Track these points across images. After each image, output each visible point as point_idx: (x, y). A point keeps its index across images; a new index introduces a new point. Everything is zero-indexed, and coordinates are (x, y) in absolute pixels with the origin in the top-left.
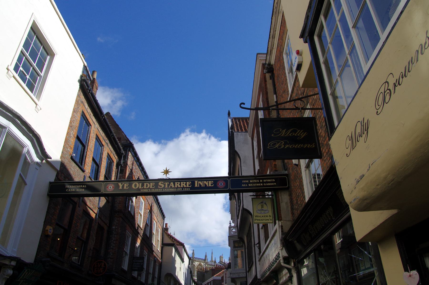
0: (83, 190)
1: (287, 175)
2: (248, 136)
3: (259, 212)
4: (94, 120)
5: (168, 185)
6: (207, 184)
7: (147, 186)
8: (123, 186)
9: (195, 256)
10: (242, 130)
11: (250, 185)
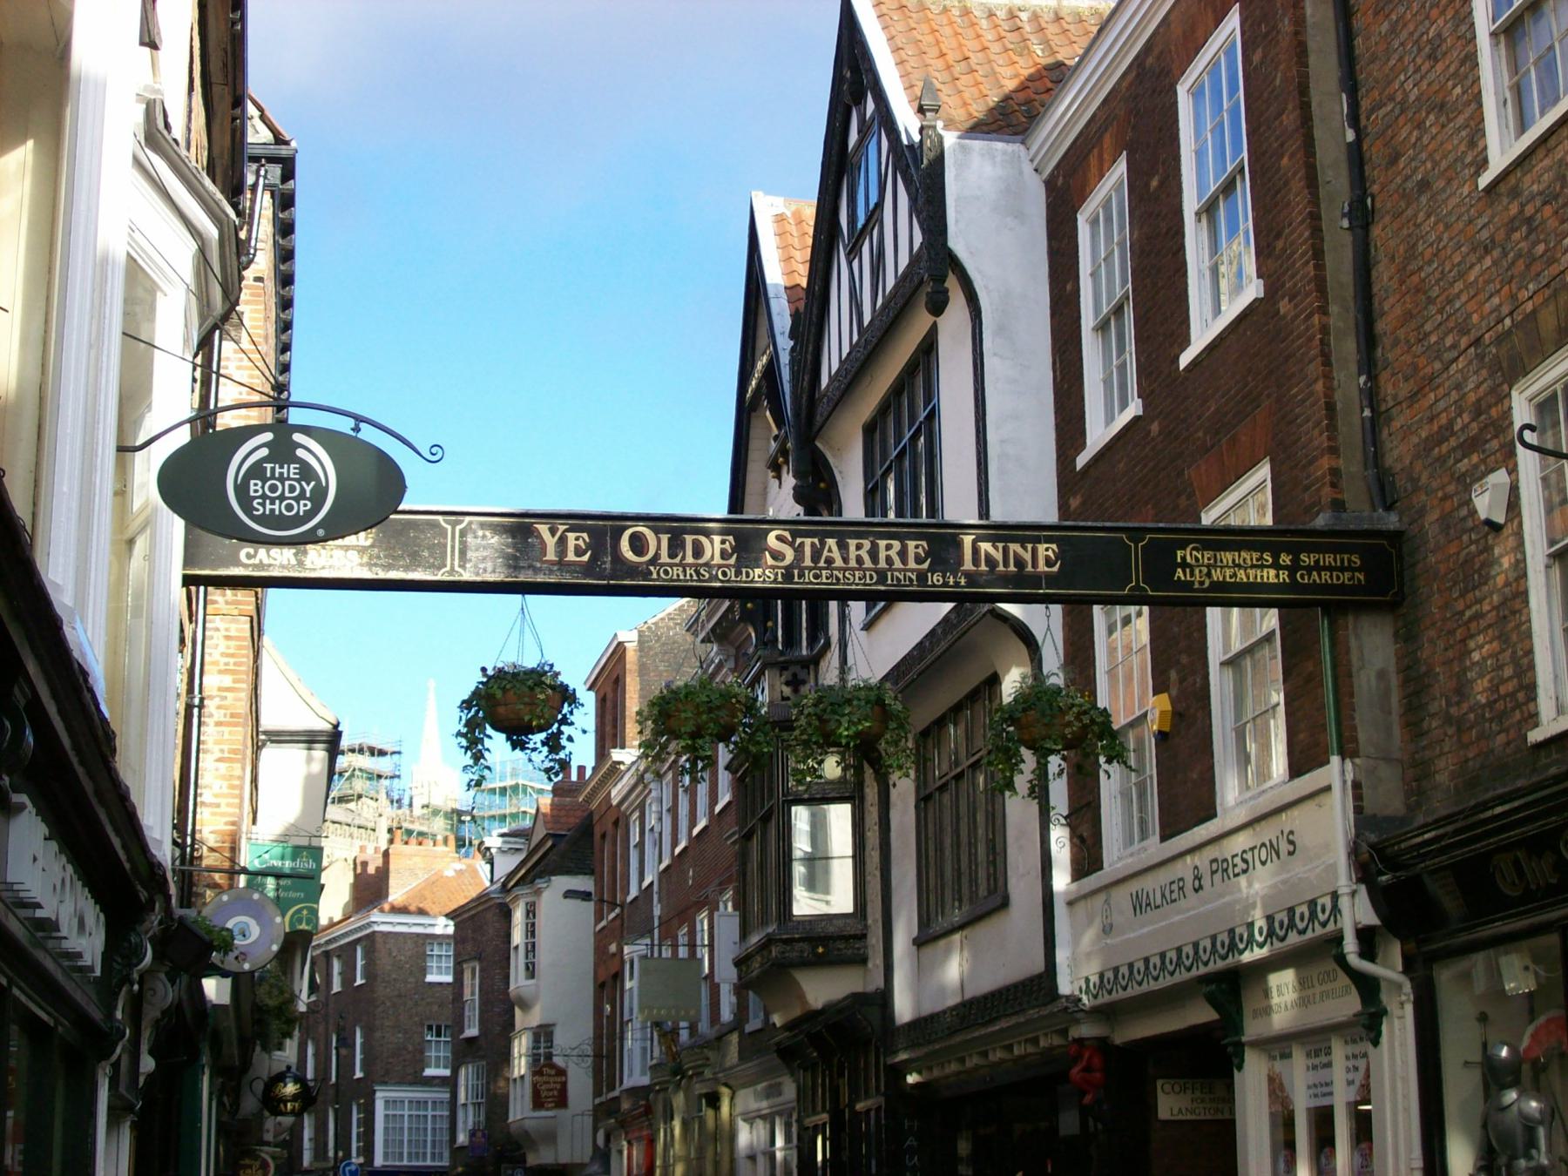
1: (1396, 537)
5: (816, 555)
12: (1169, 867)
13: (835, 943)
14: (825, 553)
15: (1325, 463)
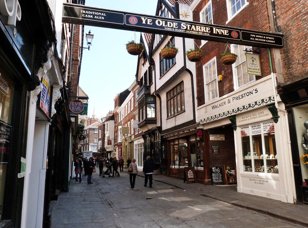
3: (251, 65)
8: (146, 21)
12: (222, 100)
13: (153, 121)
15: (268, 25)
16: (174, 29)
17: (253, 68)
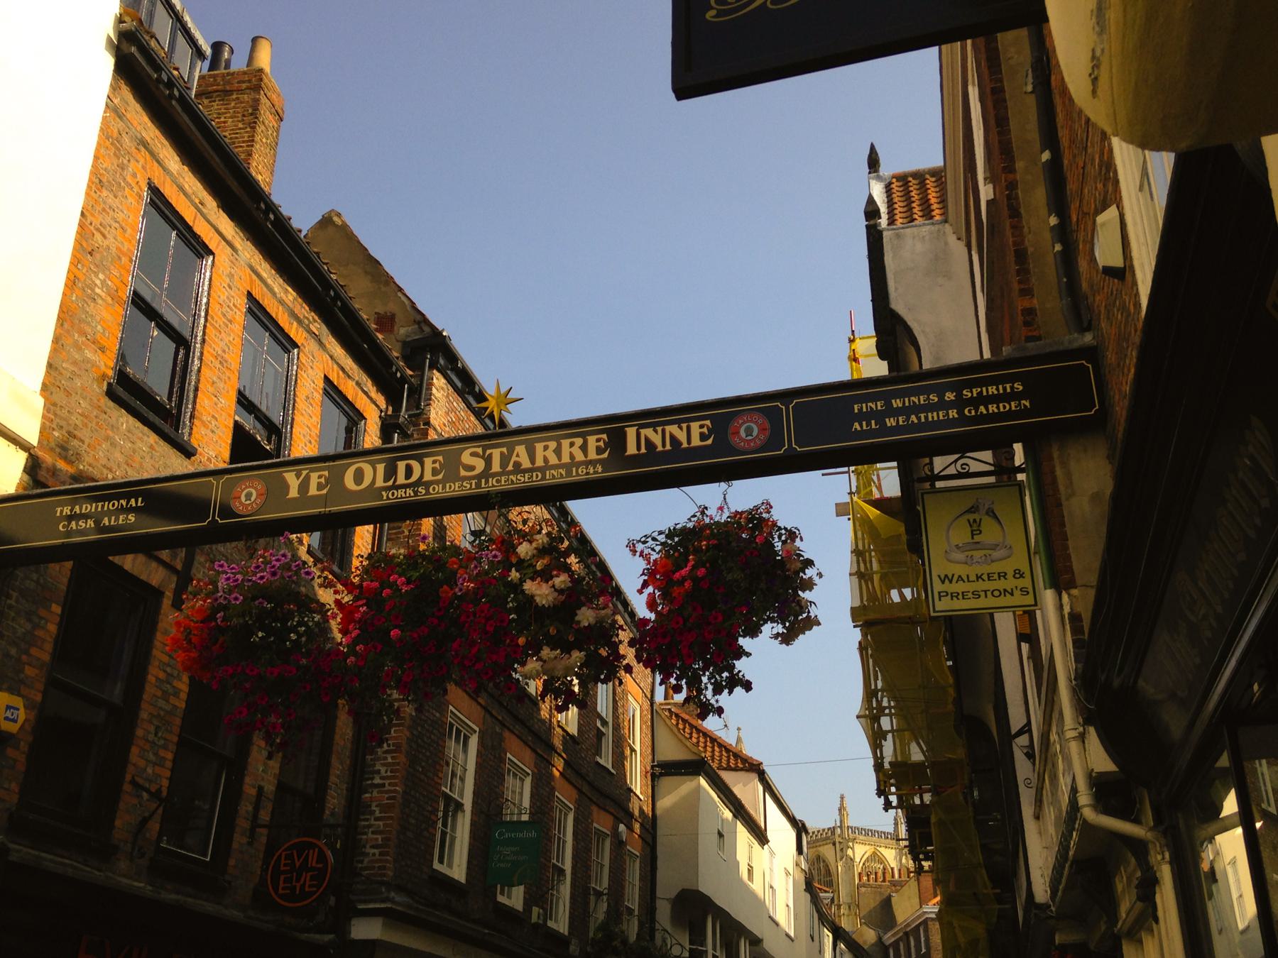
0: (132, 518)
1: (1092, 353)
2: (952, 239)
3: (960, 556)
4: (227, 226)
5: (505, 460)
6: (682, 436)
7: (409, 471)
8: (304, 486)
9: (851, 821)
10: (928, 214)
11: (890, 422)
14: (514, 458)
16: (427, 490)
17: (973, 571)
